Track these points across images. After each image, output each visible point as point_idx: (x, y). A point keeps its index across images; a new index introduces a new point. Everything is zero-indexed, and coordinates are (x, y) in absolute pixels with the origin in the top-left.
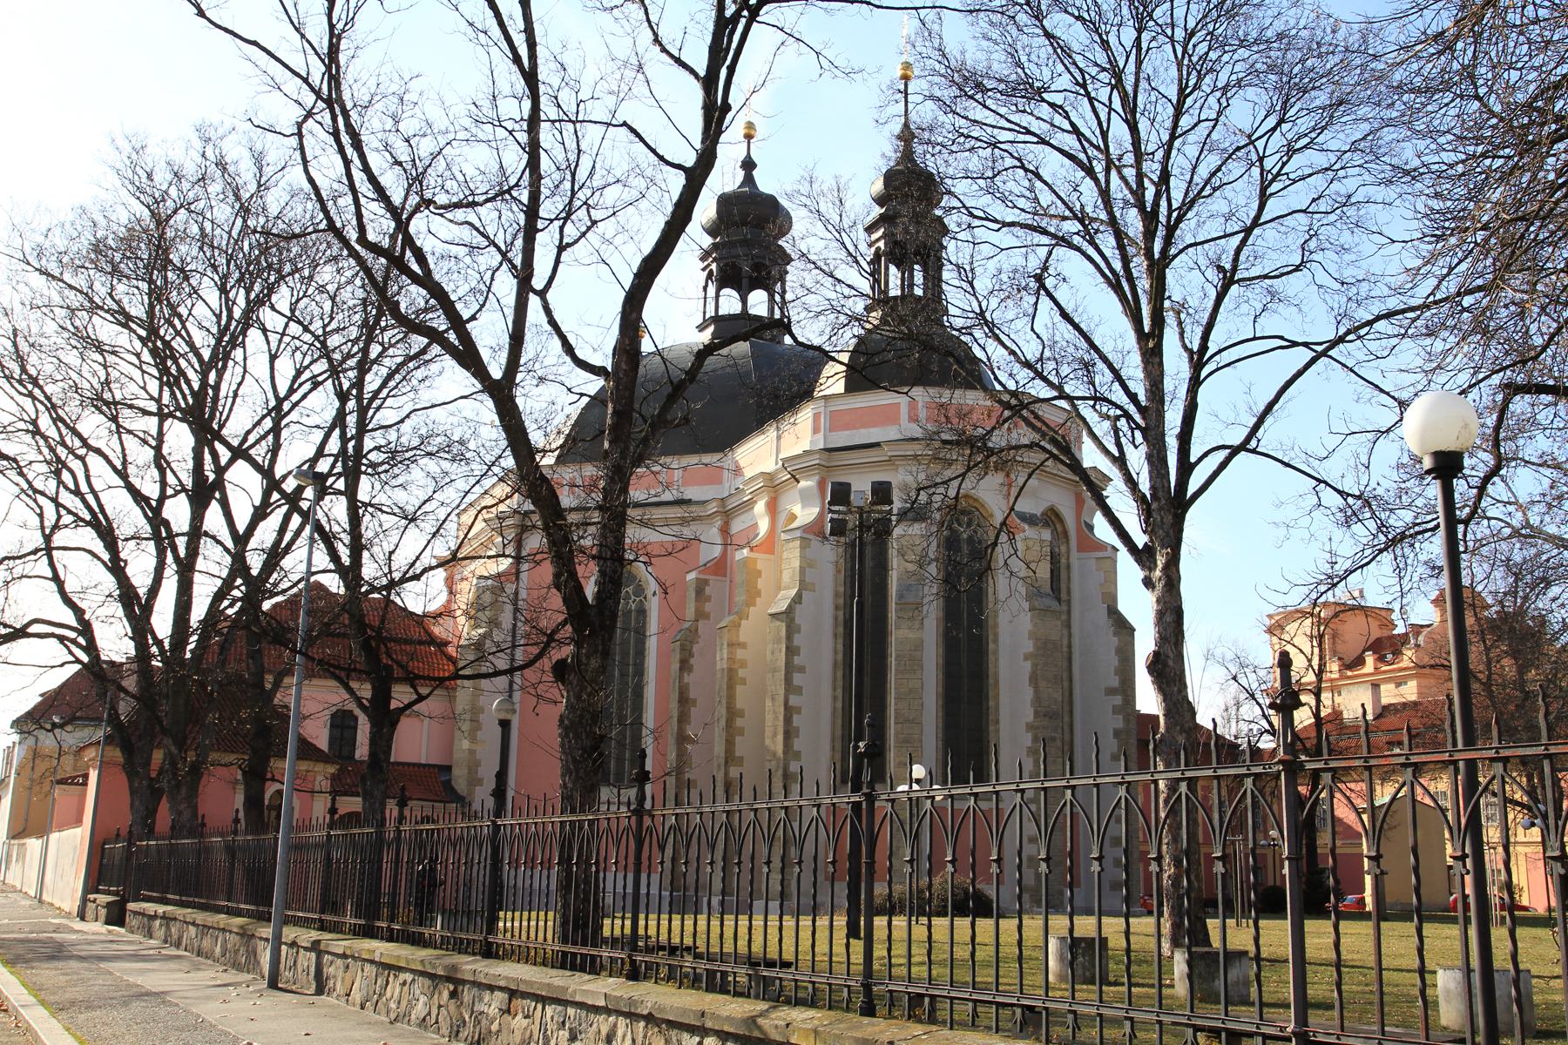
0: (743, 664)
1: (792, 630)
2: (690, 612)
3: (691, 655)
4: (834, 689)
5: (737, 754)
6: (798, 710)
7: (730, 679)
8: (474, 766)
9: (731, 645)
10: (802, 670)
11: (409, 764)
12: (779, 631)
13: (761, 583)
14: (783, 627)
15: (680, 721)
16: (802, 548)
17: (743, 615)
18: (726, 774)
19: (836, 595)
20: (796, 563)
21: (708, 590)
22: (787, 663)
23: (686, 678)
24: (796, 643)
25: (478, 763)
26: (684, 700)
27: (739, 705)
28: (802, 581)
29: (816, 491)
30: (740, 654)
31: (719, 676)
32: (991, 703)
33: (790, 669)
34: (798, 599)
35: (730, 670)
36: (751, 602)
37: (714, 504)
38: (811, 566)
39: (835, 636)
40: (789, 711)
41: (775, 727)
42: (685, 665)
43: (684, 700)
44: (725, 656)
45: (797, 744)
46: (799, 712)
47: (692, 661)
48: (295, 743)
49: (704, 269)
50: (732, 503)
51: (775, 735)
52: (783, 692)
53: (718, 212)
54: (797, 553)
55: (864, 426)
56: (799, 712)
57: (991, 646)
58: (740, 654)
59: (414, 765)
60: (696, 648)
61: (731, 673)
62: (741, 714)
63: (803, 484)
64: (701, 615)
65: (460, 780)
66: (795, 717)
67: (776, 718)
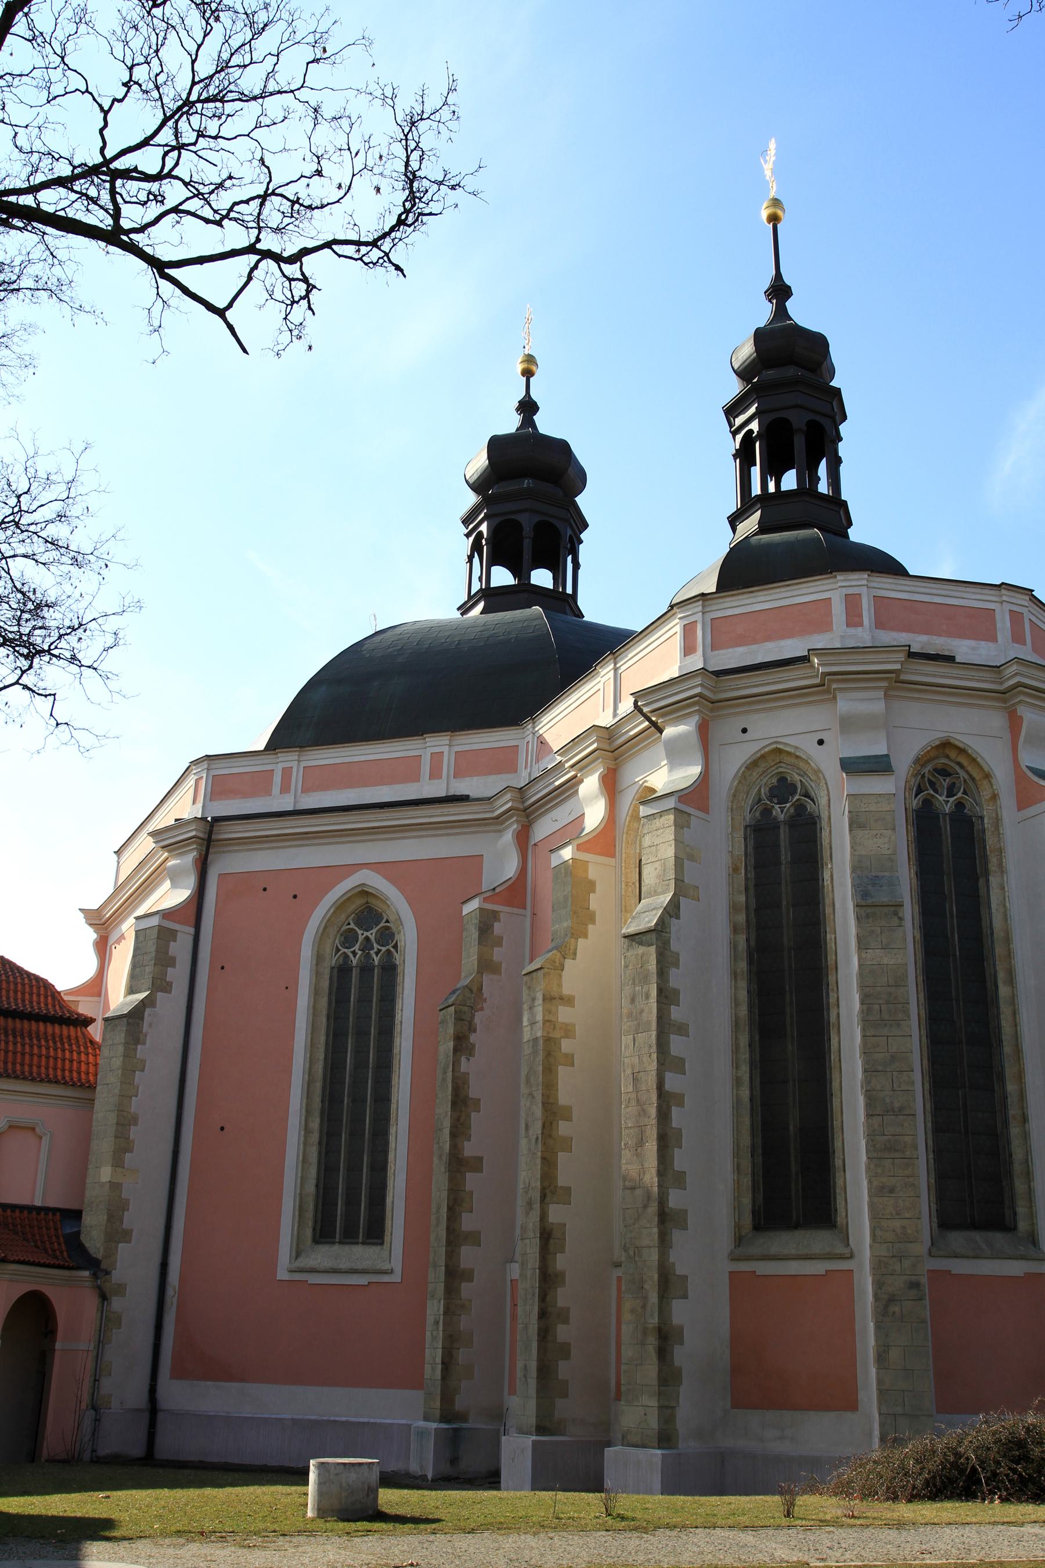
0: (569, 1031)
1: (665, 962)
2: (470, 959)
3: (472, 1029)
4: (736, 1065)
5: (561, 1182)
6: (679, 1099)
7: (548, 1054)
8: (117, 1209)
9: (548, 999)
10: (682, 1030)
11: (14, 1207)
12: (643, 960)
13: (595, 902)
14: (651, 953)
15: (453, 1135)
16: (679, 826)
17: (566, 952)
18: (543, 1217)
19: (734, 908)
20: (669, 852)
21: (498, 928)
22: (660, 1018)
23: (464, 1065)
24: (673, 983)
25: (124, 1206)
26: (461, 1101)
27: (563, 1098)
28: (679, 881)
29: (695, 739)
30: (564, 1014)
31: (527, 1050)
32: (1011, 1087)
33: (665, 1027)
34: (672, 910)
35: (548, 1040)
36: (579, 932)
37: (508, 796)
38: (691, 857)
39: (734, 975)
40: (666, 1100)
41: (641, 1129)
42: (462, 1045)
43: (461, 1101)
44: (539, 1017)
45: (680, 1160)
46: (681, 1104)
47: (473, 1038)
48: (862, 1396)
49: (468, 535)
50: (535, 795)
51: (641, 1143)
52: (654, 1066)
53: (489, 457)
54: (670, 834)
55: (769, 638)
56: (681, 1104)
57: (1003, 991)
58: (564, 1014)
59: (22, 1208)
60: (478, 1018)
61: (550, 1044)
62: (566, 1114)
63: (669, 731)
64: (486, 966)
65: (94, 1233)
66: (675, 1111)
67: (643, 1112)
